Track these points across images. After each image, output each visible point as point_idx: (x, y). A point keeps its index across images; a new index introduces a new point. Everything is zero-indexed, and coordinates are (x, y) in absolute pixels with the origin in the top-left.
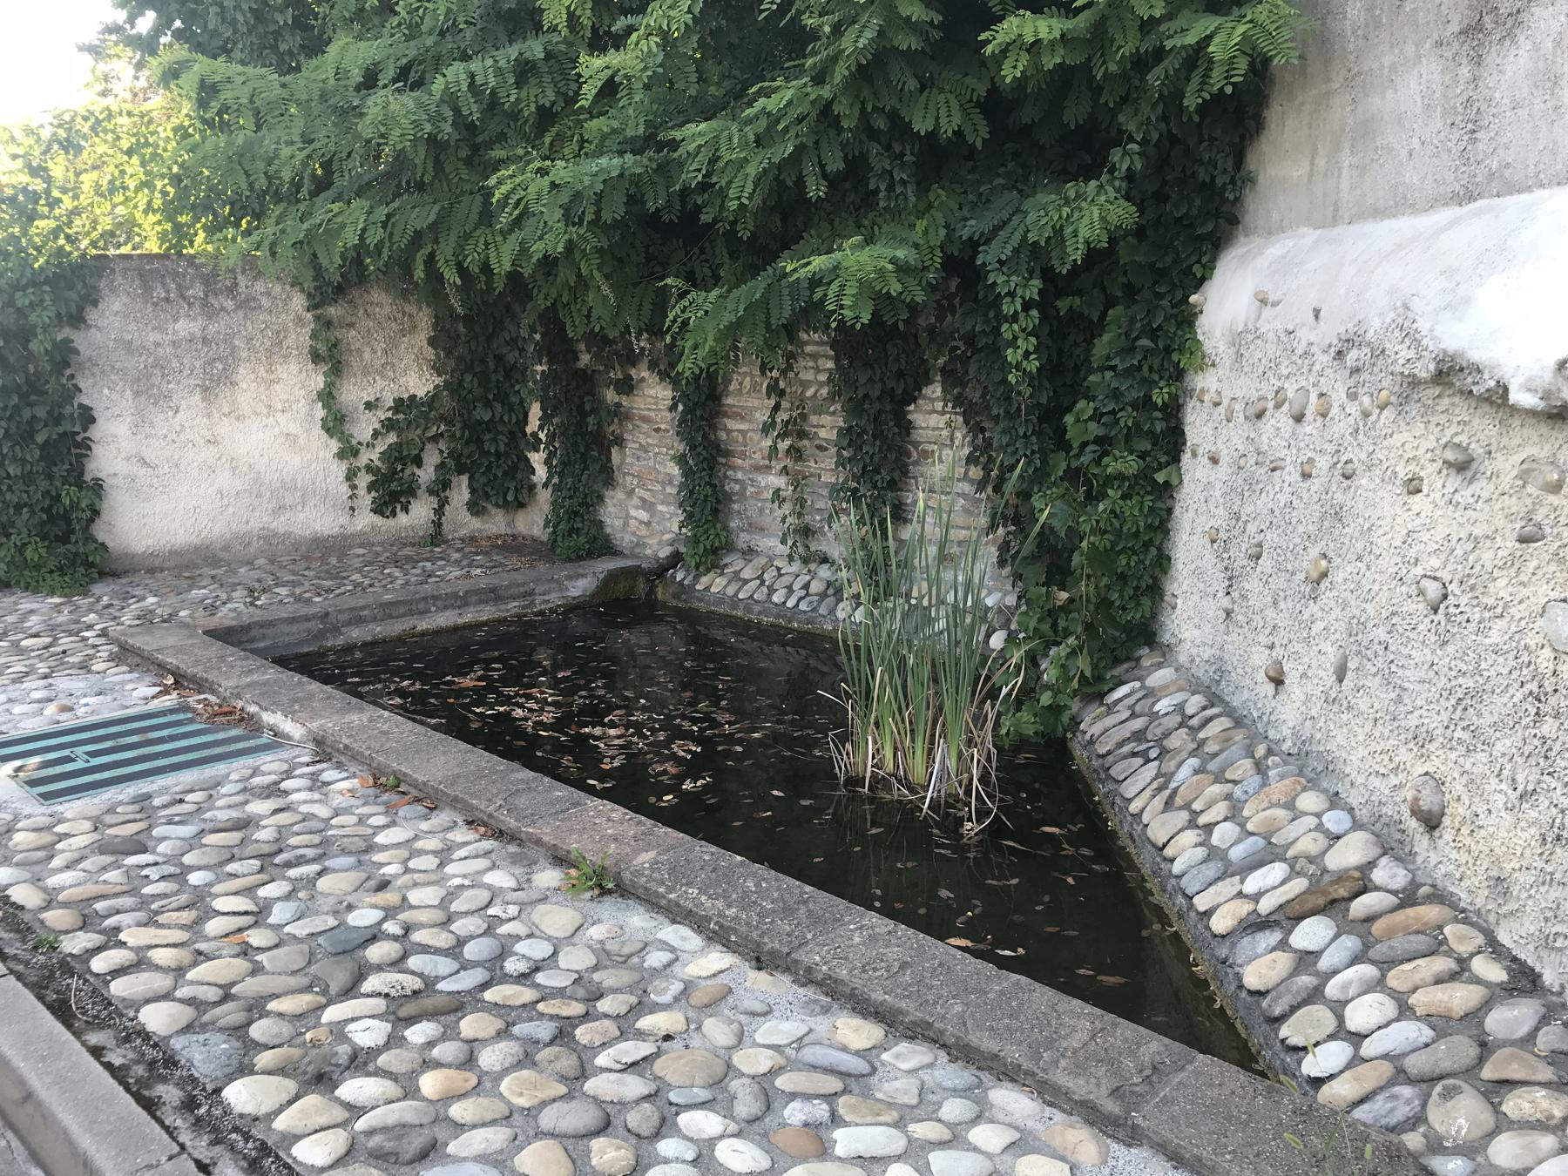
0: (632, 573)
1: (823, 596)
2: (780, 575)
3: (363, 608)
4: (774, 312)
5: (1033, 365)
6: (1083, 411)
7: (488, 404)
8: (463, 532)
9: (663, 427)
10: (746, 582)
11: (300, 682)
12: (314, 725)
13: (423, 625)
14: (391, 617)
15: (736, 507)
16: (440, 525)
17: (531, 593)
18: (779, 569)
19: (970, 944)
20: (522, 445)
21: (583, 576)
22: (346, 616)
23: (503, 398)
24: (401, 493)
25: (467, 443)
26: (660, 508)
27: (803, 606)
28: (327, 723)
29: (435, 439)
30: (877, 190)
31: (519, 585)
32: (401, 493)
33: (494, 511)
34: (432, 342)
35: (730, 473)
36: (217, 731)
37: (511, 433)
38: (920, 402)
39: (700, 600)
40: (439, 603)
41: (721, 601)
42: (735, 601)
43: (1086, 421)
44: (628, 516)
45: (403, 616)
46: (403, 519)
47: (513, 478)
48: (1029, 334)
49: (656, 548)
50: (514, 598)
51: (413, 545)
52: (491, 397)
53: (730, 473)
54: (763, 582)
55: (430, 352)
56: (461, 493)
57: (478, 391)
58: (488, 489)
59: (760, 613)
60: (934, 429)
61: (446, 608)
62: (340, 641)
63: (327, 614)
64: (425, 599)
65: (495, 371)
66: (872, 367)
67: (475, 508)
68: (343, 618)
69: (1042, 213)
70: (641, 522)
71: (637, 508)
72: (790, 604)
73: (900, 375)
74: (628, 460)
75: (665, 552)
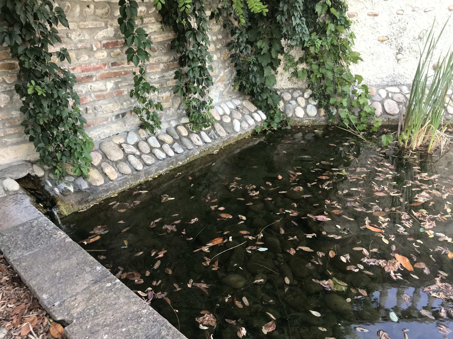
39: (107, 191)
41: (125, 181)
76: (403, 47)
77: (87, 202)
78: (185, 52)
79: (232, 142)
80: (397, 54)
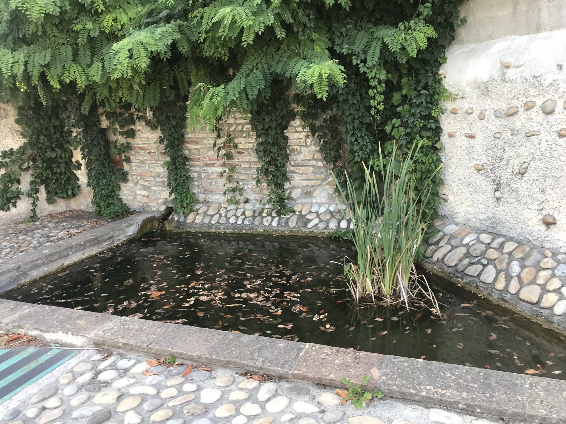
0: (151, 220)
1: (254, 217)
2: (228, 211)
3: (37, 260)
4: (249, 92)
5: (381, 107)
6: (396, 123)
7: (53, 150)
8: (46, 213)
9: (153, 151)
10: (212, 216)
11: (337, 351)
12: (92, 335)
13: (67, 262)
14: (51, 261)
15: (196, 183)
16: (35, 211)
17: (112, 237)
18: (226, 208)
19: (537, 372)
20: (72, 167)
21: (132, 225)
22: (30, 265)
23: (61, 146)
24: (12, 198)
25: (46, 169)
26: (153, 188)
27: (246, 222)
28: (96, 333)
29: (26, 170)
30: (298, 32)
31: (107, 234)
32: (12, 198)
33: (59, 200)
34: (18, 122)
35: (192, 168)
36: (18, 352)
37: (66, 162)
38: (289, 128)
39: (191, 227)
40: (73, 250)
41: (202, 226)
42: (210, 225)
43: (398, 127)
44: (136, 194)
45: (57, 259)
46: (13, 210)
47: (69, 184)
48: (381, 94)
49: (157, 207)
50: (105, 241)
51: (22, 223)
52: (54, 146)
53: (192, 168)
54: (221, 215)
55: (18, 127)
56: (43, 194)
57: (47, 144)
58: (57, 190)
59: (224, 229)
60: (297, 139)
61: (76, 251)
62: (28, 279)
63: (19, 267)
64: (66, 249)
65: (55, 133)
66: (270, 114)
67: (50, 201)
68: (27, 267)
69: (392, 38)
70: (144, 196)
71: (141, 190)
72: (239, 222)
73: (283, 117)
74: (134, 168)
75: (163, 208)
76: (501, 182)
77: (179, 228)
78: (491, 142)
79: (300, 234)
80: (496, 191)
